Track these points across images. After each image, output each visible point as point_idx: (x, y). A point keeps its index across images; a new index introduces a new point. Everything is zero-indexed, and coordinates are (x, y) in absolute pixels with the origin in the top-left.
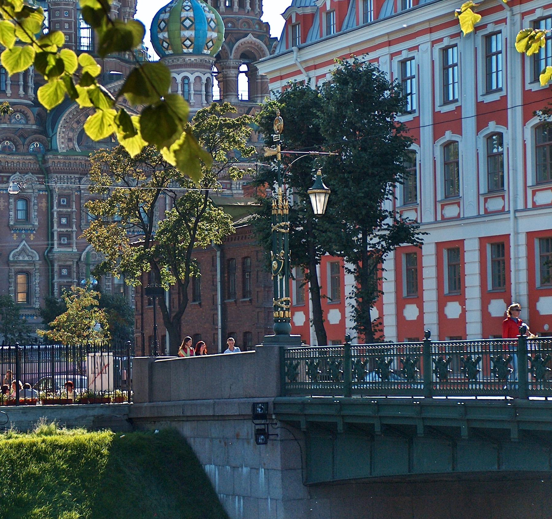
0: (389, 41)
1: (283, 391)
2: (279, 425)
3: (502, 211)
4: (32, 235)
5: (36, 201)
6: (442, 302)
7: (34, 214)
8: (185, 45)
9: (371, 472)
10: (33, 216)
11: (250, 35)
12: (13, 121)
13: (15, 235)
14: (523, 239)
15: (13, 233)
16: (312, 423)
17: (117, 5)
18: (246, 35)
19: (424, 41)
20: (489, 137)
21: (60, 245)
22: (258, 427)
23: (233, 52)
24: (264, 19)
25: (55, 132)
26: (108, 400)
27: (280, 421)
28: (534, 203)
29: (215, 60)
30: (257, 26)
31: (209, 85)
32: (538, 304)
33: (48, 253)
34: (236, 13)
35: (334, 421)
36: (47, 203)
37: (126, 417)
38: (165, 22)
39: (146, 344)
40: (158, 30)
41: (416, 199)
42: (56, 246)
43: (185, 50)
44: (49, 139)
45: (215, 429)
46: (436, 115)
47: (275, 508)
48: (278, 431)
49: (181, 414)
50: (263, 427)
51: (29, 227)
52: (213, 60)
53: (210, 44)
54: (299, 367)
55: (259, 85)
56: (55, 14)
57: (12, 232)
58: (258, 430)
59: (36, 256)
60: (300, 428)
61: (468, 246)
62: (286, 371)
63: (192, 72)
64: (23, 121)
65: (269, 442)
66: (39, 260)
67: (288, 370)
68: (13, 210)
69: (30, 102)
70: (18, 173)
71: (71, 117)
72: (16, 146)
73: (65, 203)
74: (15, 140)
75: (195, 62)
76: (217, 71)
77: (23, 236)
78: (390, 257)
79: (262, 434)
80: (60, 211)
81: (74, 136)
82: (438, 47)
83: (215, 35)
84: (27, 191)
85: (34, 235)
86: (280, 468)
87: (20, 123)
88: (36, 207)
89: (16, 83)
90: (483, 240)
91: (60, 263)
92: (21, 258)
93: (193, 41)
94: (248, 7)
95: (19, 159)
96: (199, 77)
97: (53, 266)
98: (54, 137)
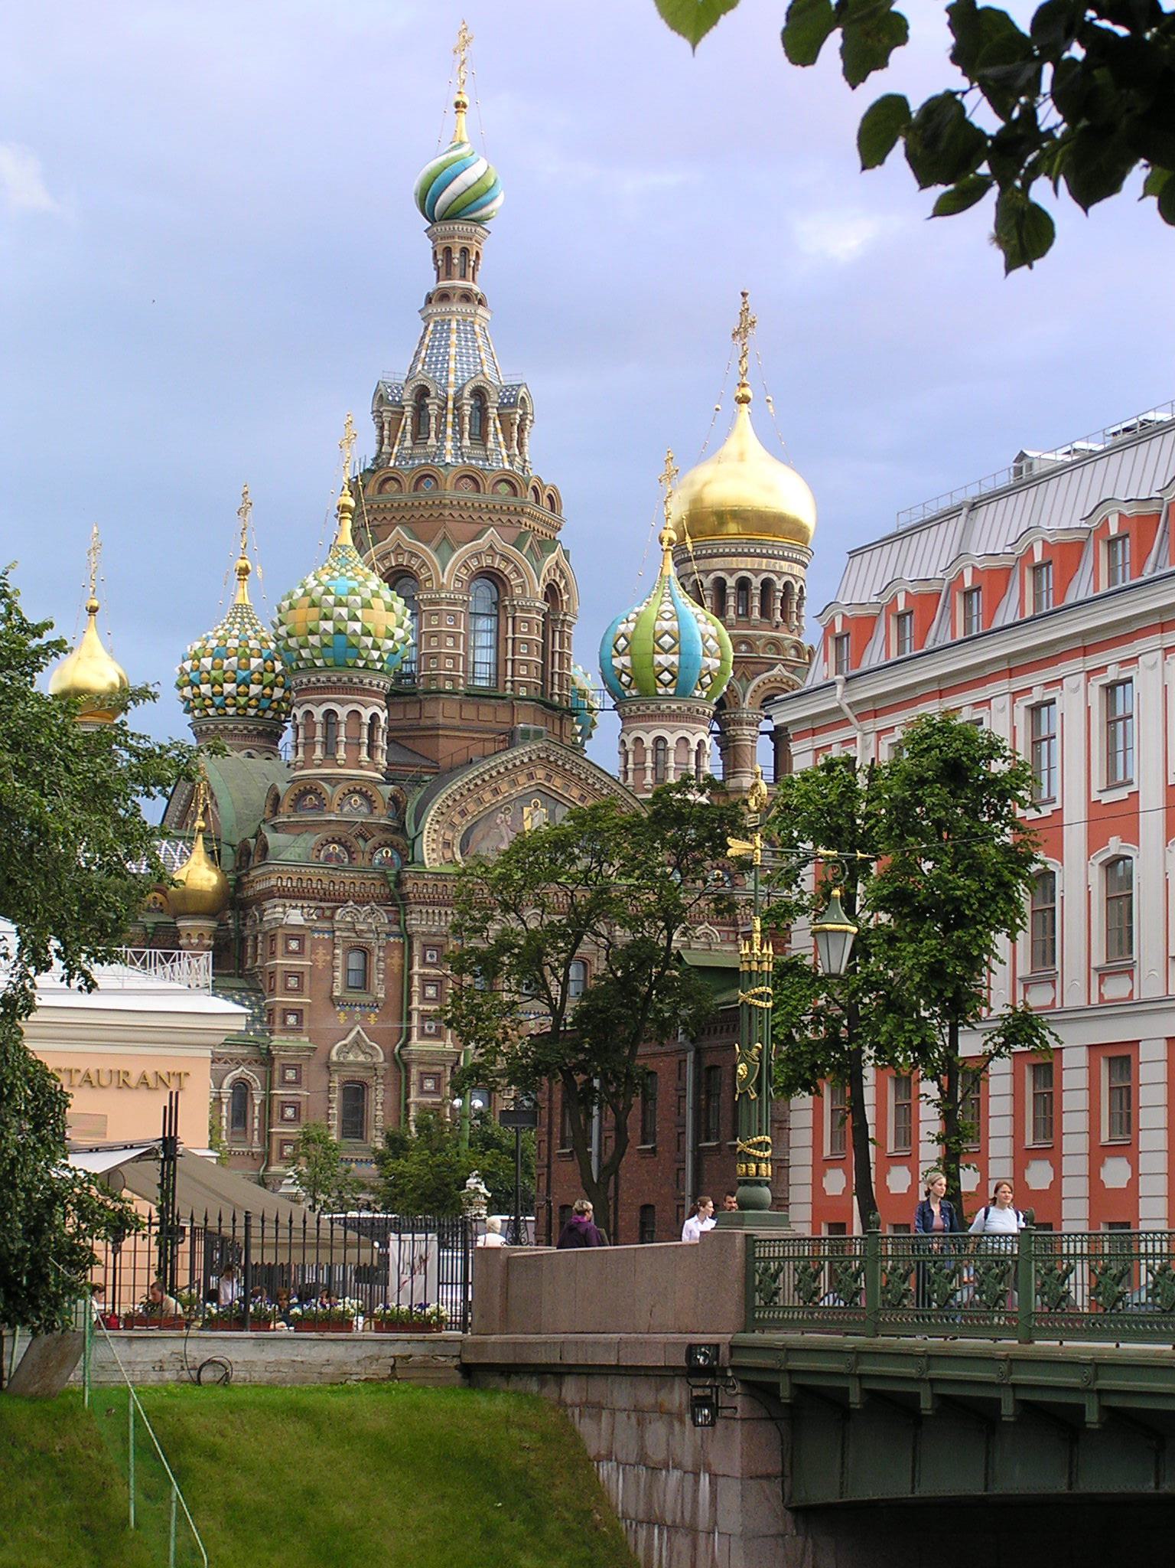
0: (1011, 670)
1: (750, 1323)
2: (739, 1389)
4: (372, 1015)
5: (381, 954)
6: (1098, 1154)
7: (377, 978)
8: (660, 681)
9: (913, 1488)
10: (376, 982)
11: (780, 666)
12: (346, 808)
13: (342, 1014)
15: (339, 1012)
16: (801, 1388)
17: (542, 607)
18: (772, 666)
21: (423, 1035)
22: (697, 1392)
23: (748, 695)
25: (419, 829)
26: (440, 1323)
27: (741, 1381)
29: (714, 709)
30: (793, 652)
33: (401, 1047)
34: (755, 628)
35: (843, 1385)
36: (403, 958)
37: (456, 1362)
38: (626, 639)
39: (555, 1221)
40: (614, 652)
41: (1054, 962)
44: (409, 842)
45: (621, 1394)
47: (726, 1549)
48: (738, 1401)
49: (558, 1361)
50: (708, 1391)
51: (366, 999)
53: (707, 680)
54: (781, 1275)
56: (430, 620)
57: (338, 1008)
58: (697, 1397)
59: (378, 1054)
60: (780, 1399)
61: (1145, 1052)
62: (757, 1283)
63: (672, 730)
64: (365, 810)
65: (720, 1423)
66: (385, 1061)
67: (760, 1282)
68: (340, 970)
69: (379, 776)
70: (351, 903)
71: (450, 803)
72: (350, 854)
73: (435, 960)
74: (349, 844)
75: (678, 711)
76: (718, 729)
77: (358, 1017)
78: (1000, 1067)
79: (705, 1407)
80: (424, 974)
81: (454, 837)
84: (366, 935)
85: (377, 1015)
86: (739, 1475)
87: (359, 814)
88: (382, 965)
89: (355, 741)
91: (421, 1068)
92: (351, 1057)
93: (676, 674)
95: (354, 878)
97: (408, 1071)
98: (418, 839)
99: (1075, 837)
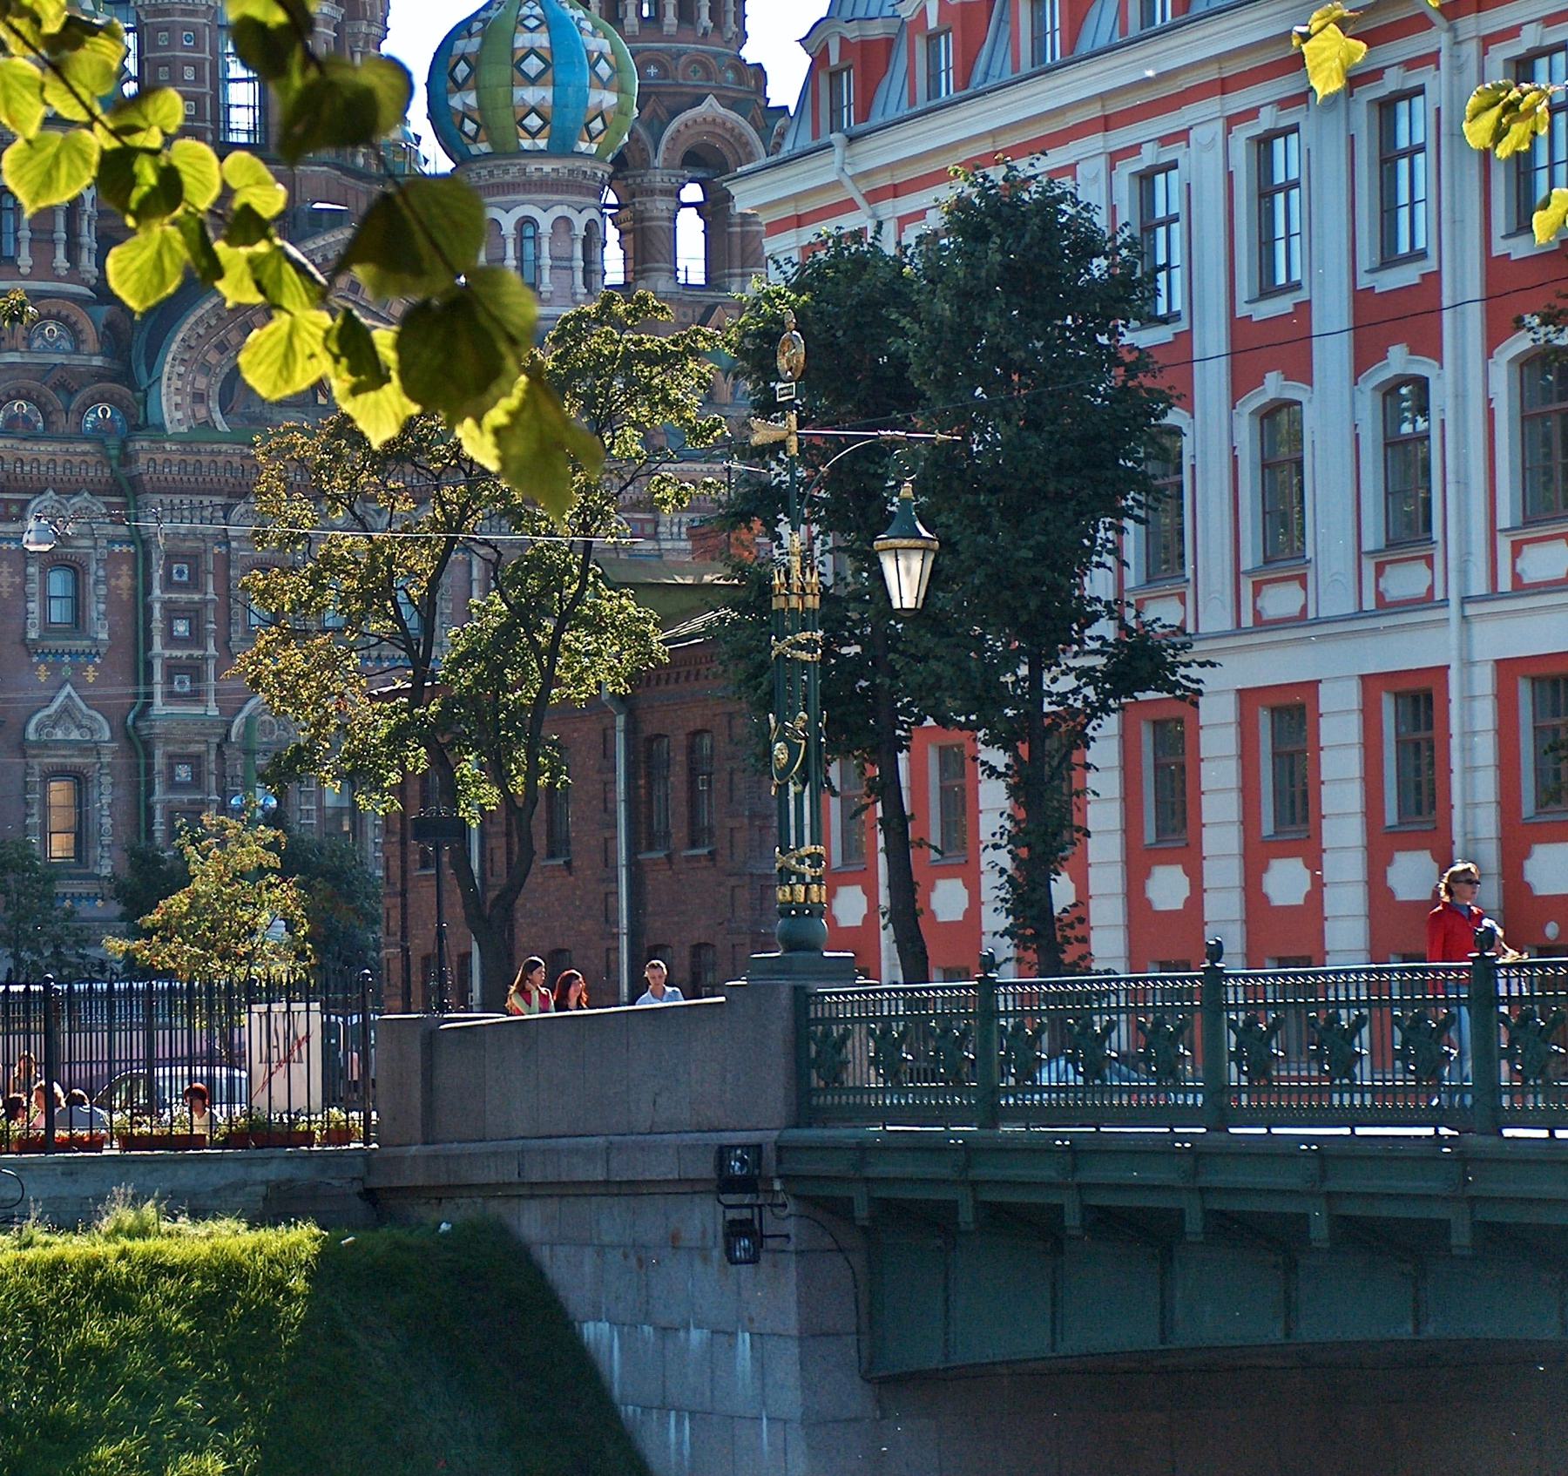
0: (1106, 117)
1: (805, 1111)
2: (792, 1207)
3: (1427, 600)
4: (91, 668)
5: (101, 573)
6: (1255, 860)
7: (96, 609)
8: (525, 128)
9: (1054, 1343)
10: (94, 615)
11: (711, 99)
12: (37, 343)
13: (42, 668)
14: (1484, 681)
15: (38, 664)
16: (886, 1203)
17: (334, 13)
18: (698, 101)
19: (1204, 116)
20: (1390, 391)
21: (171, 696)
22: (732, 1214)
23: (662, 147)
24: (750, 54)
25: (155, 375)
26: (308, 1137)
27: (796, 1196)
28: (1516, 577)
29: (610, 169)
30: (730, 75)
31: (592, 241)
32: (1529, 865)
33: (136, 718)
34: (670, 38)
35: (950, 1196)
36: (135, 576)
37: (357, 1187)
38: (468, 63)
39: (416, 978)
40: (450, 84)
41: (1183, 565)
42: (158, 700)
43: (526, 144)
44: (139, 395)
45: (611, 1221)
46: (1238, 326)
47: (780, 1444)
48: (790, 1227)
49: (515, 1178)
50: (746, 1214)
51: (82, 644)
52: (604, 170)
53: (597, 125)
54: (849, 1043)
55: (737, 241)
56: (155, 39)
57: (35, 659)
58: (732, 1222)
59: (101, 728)
60: (854, 1218)
61: (1328, 699)
62: (813, 1054)
63: (545, 206)
64: (66, 345)
65: (764, 1257)
66: (112, 740)
67: (818, 1053)
68: (37, 598)
69: (86, 291)
70: (51, 493)
71: (202, 331)
72: (46, 416)
73: (185, 578)
74: (43, 400)
75: (554, 175)
76: (616, 202)
77: (67, 672)
78: (1107, 730)
79: (745, 1236)
80: (170, 601)
81: (209, 386)
82: (1244, 133)
83: (609, 99)
84: (76, 543)
85: (97, 667)
86: (795, 1332)
87: (58, 351)
88: (102, 590)
89: (46, 237)
90: (1371, 684)
91: (170, 748)
92: (59, 734)
93: (549, 117)
94: (705, 19)
95: (54, 453)
96: (566, 220)
97: (150, 755)
98: (154, 389)
99: (1211, 379)
